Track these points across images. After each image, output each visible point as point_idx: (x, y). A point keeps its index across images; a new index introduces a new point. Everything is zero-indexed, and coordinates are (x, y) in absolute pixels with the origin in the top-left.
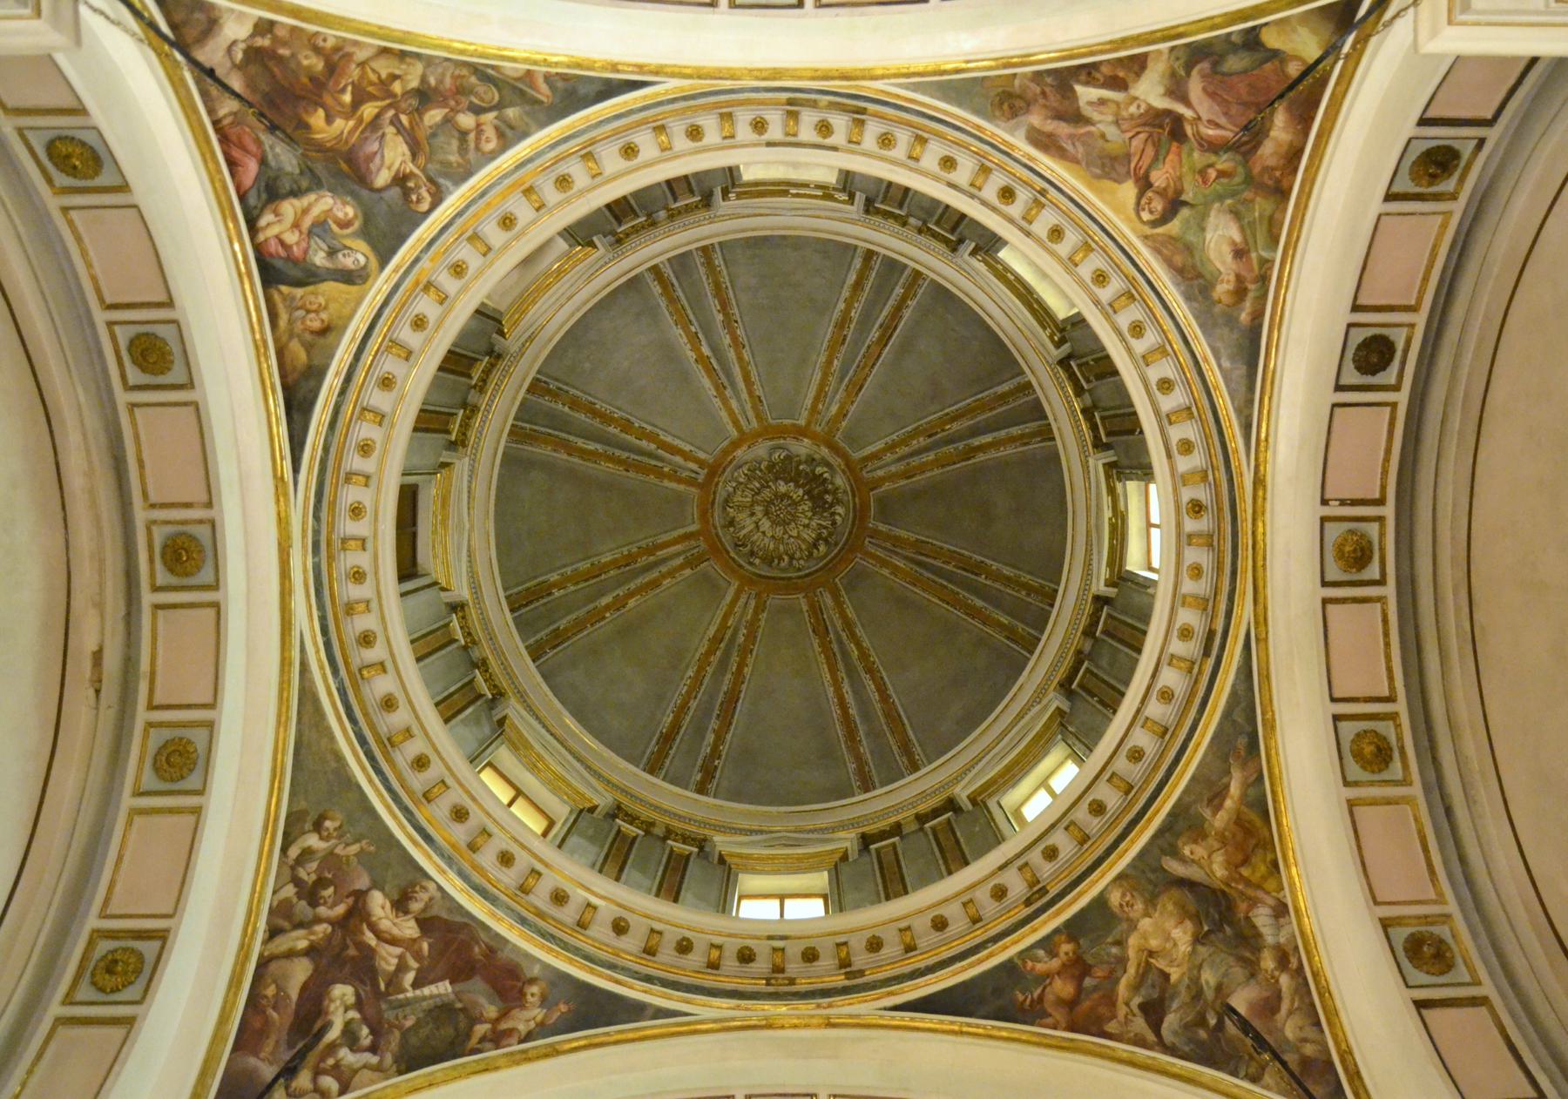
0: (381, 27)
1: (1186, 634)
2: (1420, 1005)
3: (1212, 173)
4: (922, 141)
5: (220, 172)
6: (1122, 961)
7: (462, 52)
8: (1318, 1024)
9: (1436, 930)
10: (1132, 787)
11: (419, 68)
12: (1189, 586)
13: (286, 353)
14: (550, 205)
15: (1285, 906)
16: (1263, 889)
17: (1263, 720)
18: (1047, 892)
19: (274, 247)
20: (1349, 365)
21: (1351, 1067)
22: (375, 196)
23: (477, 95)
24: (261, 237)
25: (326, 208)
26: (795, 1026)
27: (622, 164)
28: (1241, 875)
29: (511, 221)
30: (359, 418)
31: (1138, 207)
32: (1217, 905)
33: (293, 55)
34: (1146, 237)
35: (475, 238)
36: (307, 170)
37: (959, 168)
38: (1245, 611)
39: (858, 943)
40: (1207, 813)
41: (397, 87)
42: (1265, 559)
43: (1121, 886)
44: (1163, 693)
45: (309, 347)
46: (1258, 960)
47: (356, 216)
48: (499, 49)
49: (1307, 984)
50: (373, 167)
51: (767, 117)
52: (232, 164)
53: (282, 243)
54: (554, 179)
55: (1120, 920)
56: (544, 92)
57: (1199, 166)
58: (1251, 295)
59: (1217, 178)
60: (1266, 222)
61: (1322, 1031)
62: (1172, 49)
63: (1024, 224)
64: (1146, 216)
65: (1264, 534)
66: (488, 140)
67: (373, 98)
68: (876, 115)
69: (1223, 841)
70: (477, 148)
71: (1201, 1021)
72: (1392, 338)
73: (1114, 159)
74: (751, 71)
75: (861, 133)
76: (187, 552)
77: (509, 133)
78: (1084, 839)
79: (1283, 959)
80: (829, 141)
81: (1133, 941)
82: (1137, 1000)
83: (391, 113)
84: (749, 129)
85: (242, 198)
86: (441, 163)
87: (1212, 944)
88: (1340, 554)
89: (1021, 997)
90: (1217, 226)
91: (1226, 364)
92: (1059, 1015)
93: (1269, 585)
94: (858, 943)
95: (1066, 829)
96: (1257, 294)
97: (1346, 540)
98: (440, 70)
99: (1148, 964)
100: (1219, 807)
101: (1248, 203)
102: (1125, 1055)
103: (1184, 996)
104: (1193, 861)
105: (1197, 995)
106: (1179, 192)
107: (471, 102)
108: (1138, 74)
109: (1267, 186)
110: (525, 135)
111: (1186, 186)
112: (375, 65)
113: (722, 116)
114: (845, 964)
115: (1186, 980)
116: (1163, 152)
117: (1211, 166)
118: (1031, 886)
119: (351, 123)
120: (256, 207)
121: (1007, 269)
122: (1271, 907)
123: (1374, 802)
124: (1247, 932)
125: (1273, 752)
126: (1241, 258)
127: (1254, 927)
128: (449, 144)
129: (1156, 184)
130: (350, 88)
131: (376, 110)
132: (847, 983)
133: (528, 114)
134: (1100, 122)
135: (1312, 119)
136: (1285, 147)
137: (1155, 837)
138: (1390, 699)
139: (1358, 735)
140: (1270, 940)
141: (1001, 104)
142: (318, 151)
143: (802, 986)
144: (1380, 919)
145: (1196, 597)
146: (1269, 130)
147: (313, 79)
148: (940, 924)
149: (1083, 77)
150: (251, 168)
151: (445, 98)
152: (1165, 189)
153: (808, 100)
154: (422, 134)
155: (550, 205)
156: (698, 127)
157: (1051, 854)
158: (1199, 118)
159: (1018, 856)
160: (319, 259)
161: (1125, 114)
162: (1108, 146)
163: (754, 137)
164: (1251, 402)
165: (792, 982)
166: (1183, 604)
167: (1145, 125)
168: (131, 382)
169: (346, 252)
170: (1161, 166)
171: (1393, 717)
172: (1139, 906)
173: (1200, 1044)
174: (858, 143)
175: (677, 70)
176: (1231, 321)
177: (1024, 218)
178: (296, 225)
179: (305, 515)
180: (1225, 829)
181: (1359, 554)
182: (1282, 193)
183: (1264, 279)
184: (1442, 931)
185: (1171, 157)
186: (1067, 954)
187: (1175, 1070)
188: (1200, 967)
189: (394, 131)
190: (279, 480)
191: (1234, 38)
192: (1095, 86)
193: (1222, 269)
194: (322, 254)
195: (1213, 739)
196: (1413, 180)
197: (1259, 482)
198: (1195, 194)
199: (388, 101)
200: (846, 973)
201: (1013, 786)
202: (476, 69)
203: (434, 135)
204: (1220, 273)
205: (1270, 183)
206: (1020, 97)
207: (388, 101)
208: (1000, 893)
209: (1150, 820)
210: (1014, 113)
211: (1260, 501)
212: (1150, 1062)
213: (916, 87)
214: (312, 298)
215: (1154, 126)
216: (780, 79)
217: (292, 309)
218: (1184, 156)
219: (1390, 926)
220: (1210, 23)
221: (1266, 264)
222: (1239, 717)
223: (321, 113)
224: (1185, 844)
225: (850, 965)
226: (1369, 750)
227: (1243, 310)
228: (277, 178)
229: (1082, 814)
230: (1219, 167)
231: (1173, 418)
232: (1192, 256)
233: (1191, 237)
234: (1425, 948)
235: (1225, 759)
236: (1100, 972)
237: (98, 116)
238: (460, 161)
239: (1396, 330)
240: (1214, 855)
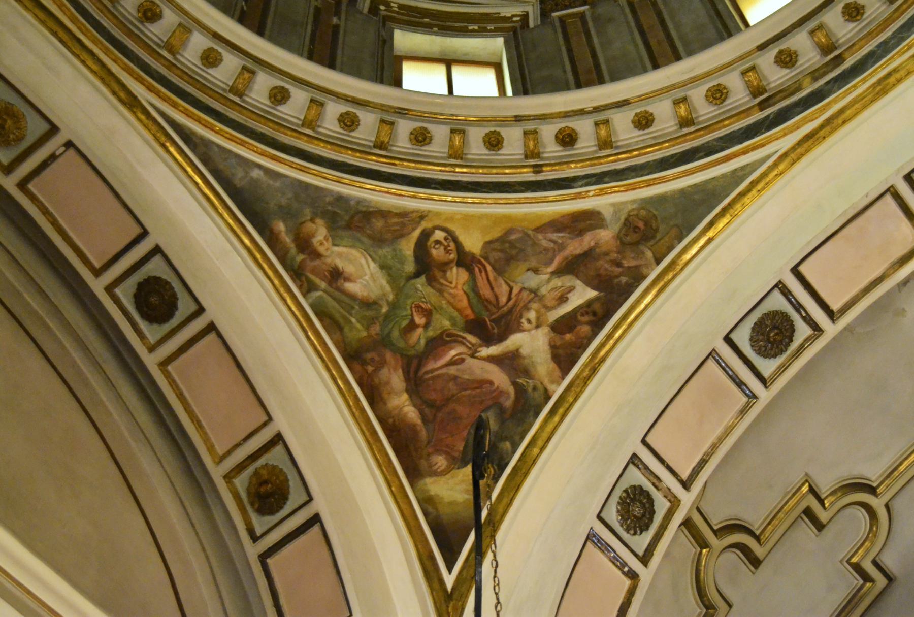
3: (420, 320)
4: (686, 122)
20: (166, 274)
31: (451, 236)
34: (422, 216)
37: (632, 126)
42: (61, 41)
57: (436, 316)
58: (293, 250)
59: (412, 321)
60: (341, 321)
62: (548, 397)
63: (530, 126)
64: (439, 235)
65: (83, 62)
68: (747, 112)
72: (155, 326)
73: (510, 260)
75: (748, 84)
80: (773, 52)
90: (374, 281)
91: (256, 173)
96: (289, 255)
101: (369, 323)
106: (431, 281)
108: (553, 347)
109: (368, 351)
111: (430, 290)
116: (474, 301)
117: (426, 326)
121: (482, 32)
126: (331, 273)
129: (455, 269)
134: (549, 281)
135: (389, 437)
136: (385, 396)
141: (646, 224)
146: (410, 397)
149: (597, 307)
152: (445, 272)
153: (825, 74)
158: (473, 356)
161: (535, 306)
162: (523, 266)
164: (205, 162)
167: (510, 311)
170: (465, 288)
174: (744, 73)
176: (287, 214)
177: (535, 132)
182: (353, 356)
183: (297, 273)
185: (465, 303)
191: (507, 445)
192: (580, 307)
193: (336, 249)
195: (97, 31)
196: (274, 467)
197: (132, 103)
198: (417, 290)
204: (335, 245)
205: (369, 356)
206: (637, 243)
210: (629, 225)
211: (116, 88)
213: (736, 177)
215: (503, 316)
218: (456, 314)
220: (542, 442)
221: (308, 288)
227: (288, 231)
230: (420, 331)
231: (246, 75)
232: (370, 237)
233: (385, 251)
239: (159, 336)
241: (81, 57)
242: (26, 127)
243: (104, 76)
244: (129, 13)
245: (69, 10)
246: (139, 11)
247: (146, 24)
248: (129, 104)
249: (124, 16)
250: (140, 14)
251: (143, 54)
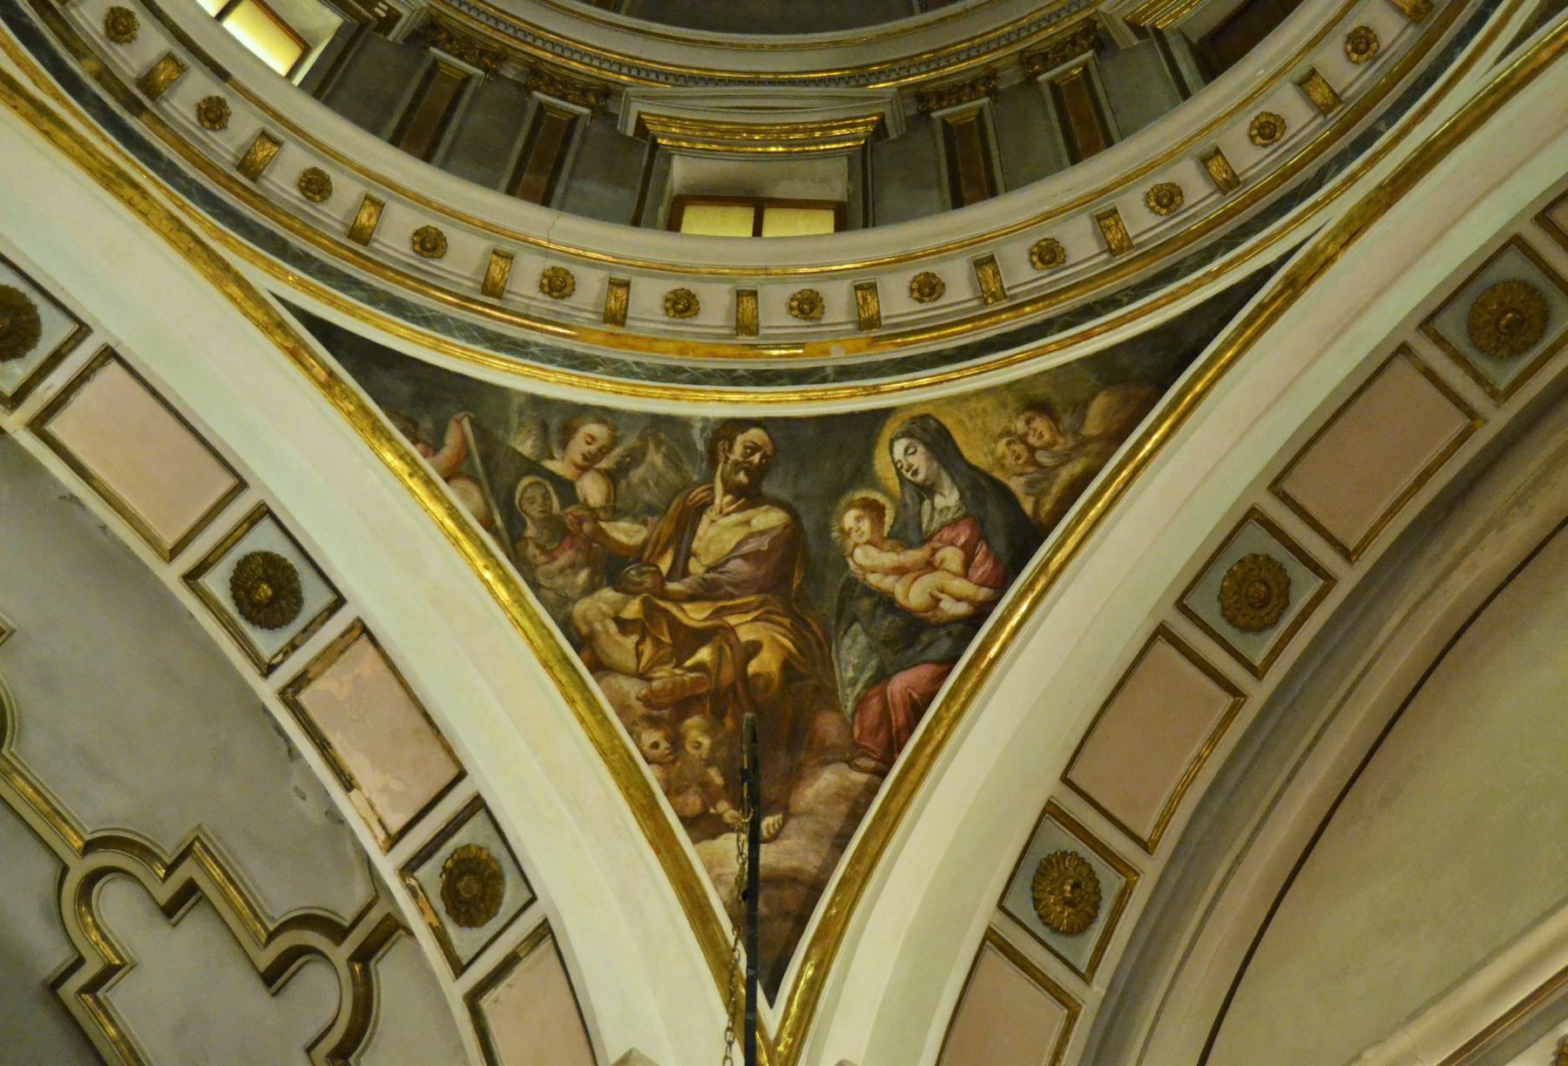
0: (571, 701)
5: (937, 718)
7: (506, 580)
11: (582, 608)
13: (1114, 427)
14: (603, 274)
19: (982, 567)
22: (801, 507)
23: (546, 509)
24: (984, 593)
25: (872, 551)
27: (455, 236)
29: (675, 303)
30: (1131, 247)
33: (709, 763)
35: (746, 326)
36: (845, 617)
41: (633, 609)
45: (1080, 408)
47: (850, 505)
48: (456, 542)
50: (764, 544)
51: (192, 116)
52: (916, 710)
53: (968, 563)
54: (566, 302)
56: (460, 431)
66: (592, 439)
67: (675, 623)
70: (614, 442)
74: (144, 214)
76: (1498, 320)
77: (554, 423)
83: (673, 586)
84: (232, 122)
85: (952, 661)
86: (677, 468)
98: (560, 581)
107: (563, 506)
110: (536, 401)
112: (631, 663)
113: (254, 176)
119: (732, 620)
120: (949, 634)
128: (644, 482)
130: (689, 663)
131: (687, 606)
133: (506, 423)
138: (1348, 555)
142: (808, 626)
147: (718, 715)
150: (900, 684)
151: (589, 540)
154: (665, 527)
155: (603, 274)
156: (303, 190)
160: (948, 498)
163: (236, 106)
168: (1317, 583)
169: (908, 475)
171: (1329, 580)
175: (249, 306)
178: (930, 566)
179: (1330, 197)
189: (692, 561)
190: (1294, 287)
194: (939, 501)
199: (662, 604)
202: (513, 542)
203: (651, 509)
207: (662, 604)
214: (1009, 461)
216: (113, 166)
217: (1048, 473)
223: (753, 667)
228: (887, 643)
237: (983, 915)
238: (652, 448)
244: (1357, 78)
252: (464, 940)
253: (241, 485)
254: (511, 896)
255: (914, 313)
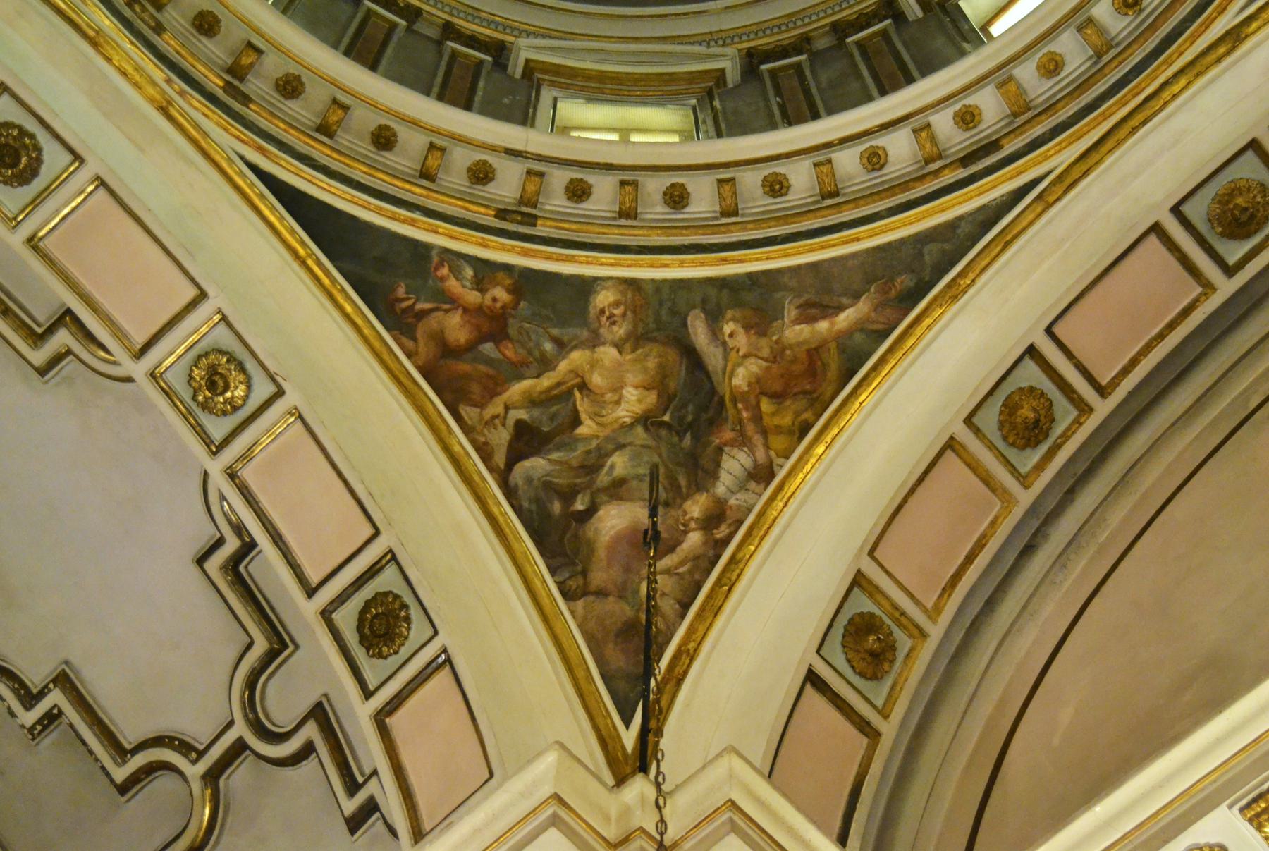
1: (967, 118)
2: (812, 678)
6: (546, 364)
8: (685, 606)
9: (898, 634)
10: (736, 214)
12: (1026, 73)
15: (772, 475)
16: (766, 438)
17: (954, 280)
18: (535, 225)
21: (679, 670)
26: (124, 74)
28: (758, 403)
32: (704, 408)
38: (1060, 157)
39: (272, 66)
40: (790, 313)
42: (1144, 123)
43: (623, 293)
44: (876, 154)
46: (688, 496)
49: (714, 563)
55: (584, 323)
61: (683, 616)
65: (1175, 96)
69: (777, 355)
71: (568, 496)
78: (628, 214)
79: (716, 517)
81: (577, 357)
82: (522, 414)
87: (658, 438)
88: (1225, 199)
89: (401, 292)
92: (425, 349)
93: (1117, 153)
94: (272, 66)
95: (623, 183)
97: (1249, 189)
99: (570, 392)
100: (811, 320)
102: (457, 448)
103: (575, 456)
104: (724, 344)
105: (591, 467)
114: (236, 71)
115: (594, 443)
118: (522, 201)
122: (755, 461)
123: (974, 466)
124: (705, 462)
125: (928, 321)
127: (718, 465)
132: (220, 94)
137: (709, 281)
138: (1102, 391)
139: (1032, 389)
140: (720, 490)
143: (168, 44)
144: (859, 571)
145: (1021, 90)
148: (384, 139)
157: (578, 192)
159: (541, 158)
165: (159, 29)
166: (1001, 85)
171: (1084, 408)
172: (620, 331)
173: (545, 515)
180: (791, 347)
181: (1244, 218)
184: (903, 642)
186: (495, 300)
187: (495, 510)
188: (621, 447)
200: (228, 83)
201: (589, 100)
208: (481, 174)
209: (724, 261)
212: (476, 478)
219: (860, 586)
222: (931, 253)
224: (734, 319)
225: (241, 79)
226: (1026, 413)
229: (654, 186)
234: (871, 638)
235: (869, 281)
236: (510, 352)
240: (752, 360)
241: (1168, 99)
242: (1248, 180)
243: (1195, 71)
244: (1129, 25)
245: (1110, 107)
246: (1126, 14)
247: (1143, 6)
248: (1235, 43)
249: (1130, 33)
250: (1130, 13)
251: (1181, 13)
252: (372, 670)
253: (1156, 229)
254: (419, 629)
255: (965, 140)
